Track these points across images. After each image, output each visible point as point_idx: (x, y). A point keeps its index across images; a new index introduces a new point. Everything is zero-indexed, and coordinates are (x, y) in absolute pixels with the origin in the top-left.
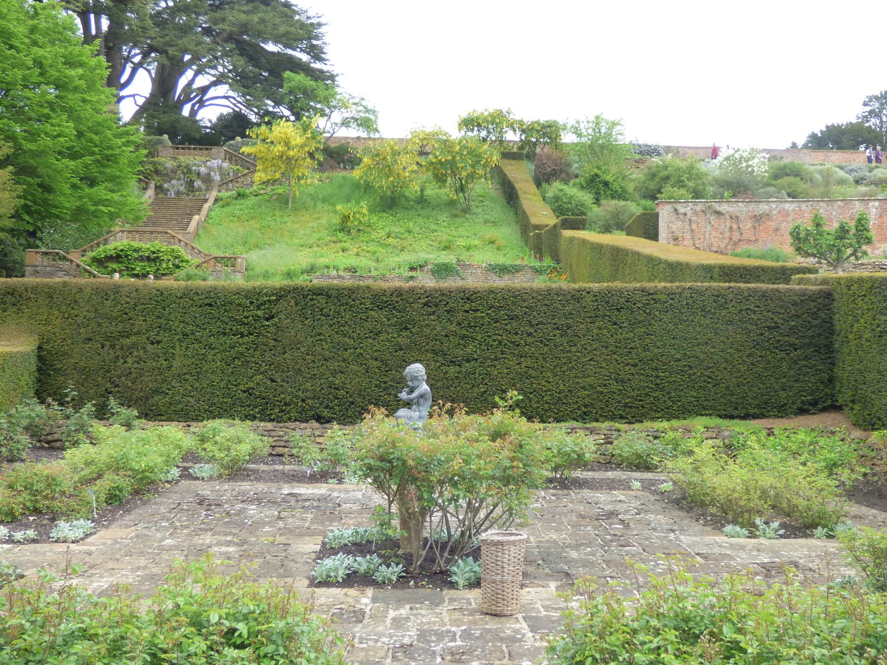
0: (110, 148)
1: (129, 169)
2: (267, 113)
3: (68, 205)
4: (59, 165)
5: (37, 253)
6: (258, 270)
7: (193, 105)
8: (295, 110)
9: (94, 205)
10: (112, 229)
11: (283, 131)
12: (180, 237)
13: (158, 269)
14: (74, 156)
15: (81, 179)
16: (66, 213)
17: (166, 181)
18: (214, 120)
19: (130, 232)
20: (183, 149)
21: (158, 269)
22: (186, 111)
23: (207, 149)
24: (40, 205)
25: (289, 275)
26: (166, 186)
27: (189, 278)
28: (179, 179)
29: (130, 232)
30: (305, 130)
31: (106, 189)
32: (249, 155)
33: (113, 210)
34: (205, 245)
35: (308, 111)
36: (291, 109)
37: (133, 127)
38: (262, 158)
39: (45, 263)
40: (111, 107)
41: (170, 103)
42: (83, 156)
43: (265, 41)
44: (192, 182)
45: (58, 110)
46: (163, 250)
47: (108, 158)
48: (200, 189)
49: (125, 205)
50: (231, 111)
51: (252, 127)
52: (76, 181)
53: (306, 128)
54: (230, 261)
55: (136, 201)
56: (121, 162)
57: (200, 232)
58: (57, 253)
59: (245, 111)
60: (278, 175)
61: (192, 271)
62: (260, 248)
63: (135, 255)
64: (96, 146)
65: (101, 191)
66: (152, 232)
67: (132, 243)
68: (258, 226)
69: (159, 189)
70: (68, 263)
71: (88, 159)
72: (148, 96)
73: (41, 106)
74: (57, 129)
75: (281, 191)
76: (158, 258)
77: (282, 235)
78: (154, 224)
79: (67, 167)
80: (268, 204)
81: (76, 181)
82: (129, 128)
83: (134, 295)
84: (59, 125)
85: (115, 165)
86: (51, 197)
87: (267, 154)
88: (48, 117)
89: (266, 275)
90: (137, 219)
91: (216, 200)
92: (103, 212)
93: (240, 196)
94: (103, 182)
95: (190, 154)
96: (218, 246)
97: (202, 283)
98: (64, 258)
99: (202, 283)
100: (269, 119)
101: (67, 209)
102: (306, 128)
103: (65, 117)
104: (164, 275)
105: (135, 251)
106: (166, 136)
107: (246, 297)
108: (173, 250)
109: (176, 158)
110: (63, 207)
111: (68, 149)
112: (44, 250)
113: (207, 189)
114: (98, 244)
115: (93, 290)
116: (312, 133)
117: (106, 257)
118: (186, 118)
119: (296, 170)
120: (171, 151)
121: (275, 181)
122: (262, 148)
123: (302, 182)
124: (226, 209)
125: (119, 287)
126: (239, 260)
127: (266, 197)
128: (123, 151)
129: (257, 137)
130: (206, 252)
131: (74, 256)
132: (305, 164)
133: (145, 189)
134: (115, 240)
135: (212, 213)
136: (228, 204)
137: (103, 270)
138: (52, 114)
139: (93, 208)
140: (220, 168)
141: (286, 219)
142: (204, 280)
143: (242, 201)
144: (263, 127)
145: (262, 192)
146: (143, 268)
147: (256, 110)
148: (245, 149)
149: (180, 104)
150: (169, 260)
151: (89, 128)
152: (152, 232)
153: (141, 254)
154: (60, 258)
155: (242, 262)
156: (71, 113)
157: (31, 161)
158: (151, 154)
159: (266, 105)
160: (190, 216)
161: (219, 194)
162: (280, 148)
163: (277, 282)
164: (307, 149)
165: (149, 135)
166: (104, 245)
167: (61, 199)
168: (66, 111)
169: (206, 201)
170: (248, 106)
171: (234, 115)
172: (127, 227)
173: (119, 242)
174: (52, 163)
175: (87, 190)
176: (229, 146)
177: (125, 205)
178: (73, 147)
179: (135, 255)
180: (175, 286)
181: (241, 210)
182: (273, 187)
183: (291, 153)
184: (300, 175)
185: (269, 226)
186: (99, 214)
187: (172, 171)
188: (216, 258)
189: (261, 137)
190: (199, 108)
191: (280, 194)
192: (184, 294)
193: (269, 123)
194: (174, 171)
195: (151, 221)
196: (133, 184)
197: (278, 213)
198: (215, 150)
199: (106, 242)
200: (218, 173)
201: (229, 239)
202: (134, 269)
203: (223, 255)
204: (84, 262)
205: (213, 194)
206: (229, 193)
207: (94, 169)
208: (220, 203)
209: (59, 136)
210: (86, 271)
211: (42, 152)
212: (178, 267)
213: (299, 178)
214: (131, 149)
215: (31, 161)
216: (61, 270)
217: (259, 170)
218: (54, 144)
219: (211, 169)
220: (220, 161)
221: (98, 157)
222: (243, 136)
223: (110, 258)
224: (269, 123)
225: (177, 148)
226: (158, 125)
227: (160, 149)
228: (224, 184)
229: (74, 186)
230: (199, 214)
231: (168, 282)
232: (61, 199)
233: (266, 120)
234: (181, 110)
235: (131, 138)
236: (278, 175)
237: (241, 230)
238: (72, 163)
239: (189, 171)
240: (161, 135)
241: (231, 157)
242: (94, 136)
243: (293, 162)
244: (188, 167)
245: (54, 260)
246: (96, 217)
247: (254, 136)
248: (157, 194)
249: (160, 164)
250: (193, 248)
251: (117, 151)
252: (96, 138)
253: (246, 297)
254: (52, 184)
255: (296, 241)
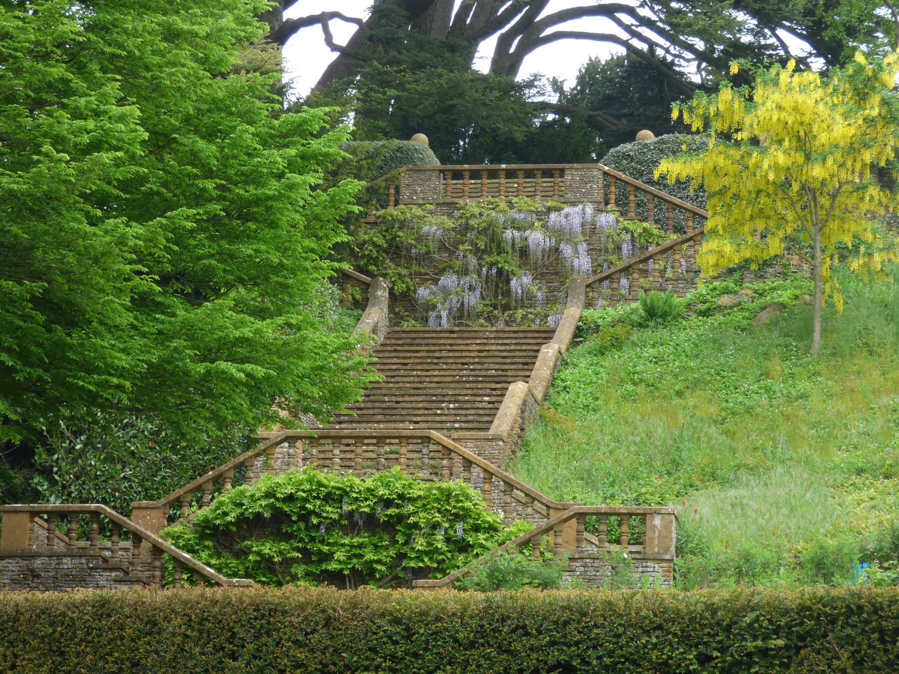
0: (252, 178)
1: (312, 244)
2: (736, 49)
3: (124, 361)
4: (98, 238)
5: (34, 514)
6: (718, 552)
7: (504, 42)
8: (827, 35)
9: (204, 359)
10: (261, 432)
11: (787, 103)
12: (469, 451)
13: (401, 556)
14: (142, 207)
15: (164, 281)
16: (119, 387)
17: (423, 279)
18: (570, 84)
19: (312, 440)
20: (475, 175)
21: (401, 556)
22: (484, 56)
23: (548, 173)
24: (41, 364)
25: (822, 567)
26: (423, 293)
27: (497, 580)
28: (464, 272)
29: (312, 440)
30: (861, 97)
31: (240, 306)
32: (681, 184)
33: (259, 371)
34: (546, 474)
35: (869, 35)
36: (814, 36)
37: (320, 111)
38: (722, 192)
39: (59, 547)
40: (254, 54)
41: (436, 35)
42: (171, 206)
43: (669, 119)
44: (504, 277)
45: (94, 67)
46: (415, 492)
47: (244, 211)
48: (527, 300)
49: (300, 354)
50: (622, 51)
51: (689, 97)
52: (148, 284)
53: (863, 88)
54: (625, 526)
55: (333, 340)
56: (284, 221)
57: (532, 433)
58: (96, 514)
59: (664, 49)
60: (775, 246)
61: (508, 559)
62: (724, 483)
63: (331, 512)
64: (209, 174)
65: (223, 315)
66: (381, 440)
67: (321, 476)
68: (713, 409)
69: (402, 302)
70: (128, 544)
71: (185, 216)
72: (365, 16)
73: (45, 57)
74: (91, 124)
75: (785, 296)
76: (400, 518)
77: (792, 439)
78: (390, 414)
79: (121, 242)
80: (746, 340)
81: (148, 284)
82: (308, 113)
83: (320, 637)
84: (97, 114)
85: (268, 233)
86: (74, 340)
87: (737, 176)
88: (64, 90)
89: (745, 568)
90: (336, 395)
91: (579, 333)
92: (231, 379)
93: (655, 315)
94: (230, 286)
95: (496, 193)
96: (587, 478)
97: (540, 595)
98: (116, 529)
99: (540, 595)
100: (741, 68)
101: (121, 373)
102: (863, 88)
103: (113, 88)
104: (419, 573)
105: (329, 498)
106: (421, 139)
107: (685, 638)
108: (448, 495)
109: (452, 205)
110: (111, 369)
111: (124, 185)
112: (55, 503)
113: (552, 299)
114: (218, 483)
115: (189, 623)
116: (885, 102)
117: (241, 520)
118: (484, 79)
119: (834, 225)
120: (438, 183)
121: (766, 264)
122: (721, 162)
123: (856, 264)
124: (613, 360)
125: (272, 612)
126: (657, 521)
127: (738, 317)
128: (292, 187)
129: (707, 125)
130: (551, 497)
131: (146, 521)
132: (865, 206)
133: (360, 305)
134: (267, 466)
135: (566, 374)
136: (617, 344)
137: (234, 563)
138: (77, 83)
139: (201, 368)
140: (591, 230)
141: (803, 385)
142: (545, 585)
143: (662, 333)
144: (726, 94)
145: (725, 300)
146: (355, 552)
147: (700, 45)
148: (670, 168)
149: (464, 40)
150: (435, 526)
151: (187, 119)
152: (381, 440)
153: (347, 508)
154: (102, 530)
155: (666, 527)
156: (131, 72)
157: (15, 229)
158: (373, 196)
159: (731, 25)
160: (498, 386)
161: (589, 313)
162: (781, 159)
163: (784, 587)
164: (868, 156)
165: (371, 135)
166: (236, 482)
167: (106, 342)
168: (119, 71)
169: (548, 335)
170: (675, 30)
171: (632, 64)
172: (307, 424)
173: (282, 474)
174: (77, 232)
175: (181, 313)
176: (617, 162)
177: (300, 354)
178: (142, 180)
179: (331, 512)
180: (452, 606)
181: (658, 360)
182: (760, 285)
183: (817, 172)
184: (848, 241)
185: (749, 410)
186: (218, 387)
187: (442, 247)
188: (581, 516)
189: (717, 125)
190: (526, 47)
191: (783, 306)
192: (481, 631)
193: (743, 80)
194: (448, 247)
195: (377, 404)
196: (319, 288)
197: (777, 367)
198: (573, 174)
199: (241, 474)
200: (583, 248)
201: (621, 453)
202: (328, 557)
203: (603, 507)
204: (176, 538)
205: (571, 314)
206: (622, 309)
207: (203, 245)
208: (592, 342)
209: (96, 146)
210: (181, 565)
211: (48, 197)
212: (463, 547)
213: (844, 253)
214: (312, 179)
215: (15, 229)
216: (107, 565)
217: (714, 232)
218: (82, 172)
219: (560, 234)
220: (589, 209)
221: (216, 208)
222: (662, 125)
223: (253, 525)
224: (743, 80)
225: (457, 175)
226: (398, 108)
227: (404, 180)
228: (602, 280)
229: (142, 303)
230: (526, 378)
231: (428, 595)
232: (106, 342)
233: (734, 69)
234: (469, 57)
235: (315, 145)
236: (775, 246)
237: (660, 428)
238: (137, 229)
239: (496, 244)
240: (408, 137)
241: (623, 196)
242: (201, 144)
243: (824, 201)
244: (491, 233)
245: (86, 535)
246: (209, 394)
247: (697, 124)
248: (395, 318)
249: (403, 225)
250: (510, 486)
251: (273, 187)
252: (208, 149)
253: (685, 638)
254: (78, 299)
255: (839, 457)
